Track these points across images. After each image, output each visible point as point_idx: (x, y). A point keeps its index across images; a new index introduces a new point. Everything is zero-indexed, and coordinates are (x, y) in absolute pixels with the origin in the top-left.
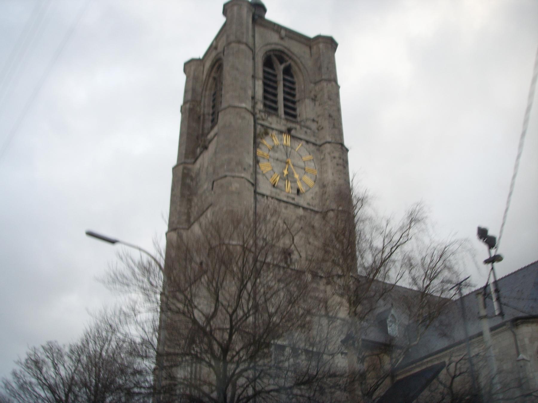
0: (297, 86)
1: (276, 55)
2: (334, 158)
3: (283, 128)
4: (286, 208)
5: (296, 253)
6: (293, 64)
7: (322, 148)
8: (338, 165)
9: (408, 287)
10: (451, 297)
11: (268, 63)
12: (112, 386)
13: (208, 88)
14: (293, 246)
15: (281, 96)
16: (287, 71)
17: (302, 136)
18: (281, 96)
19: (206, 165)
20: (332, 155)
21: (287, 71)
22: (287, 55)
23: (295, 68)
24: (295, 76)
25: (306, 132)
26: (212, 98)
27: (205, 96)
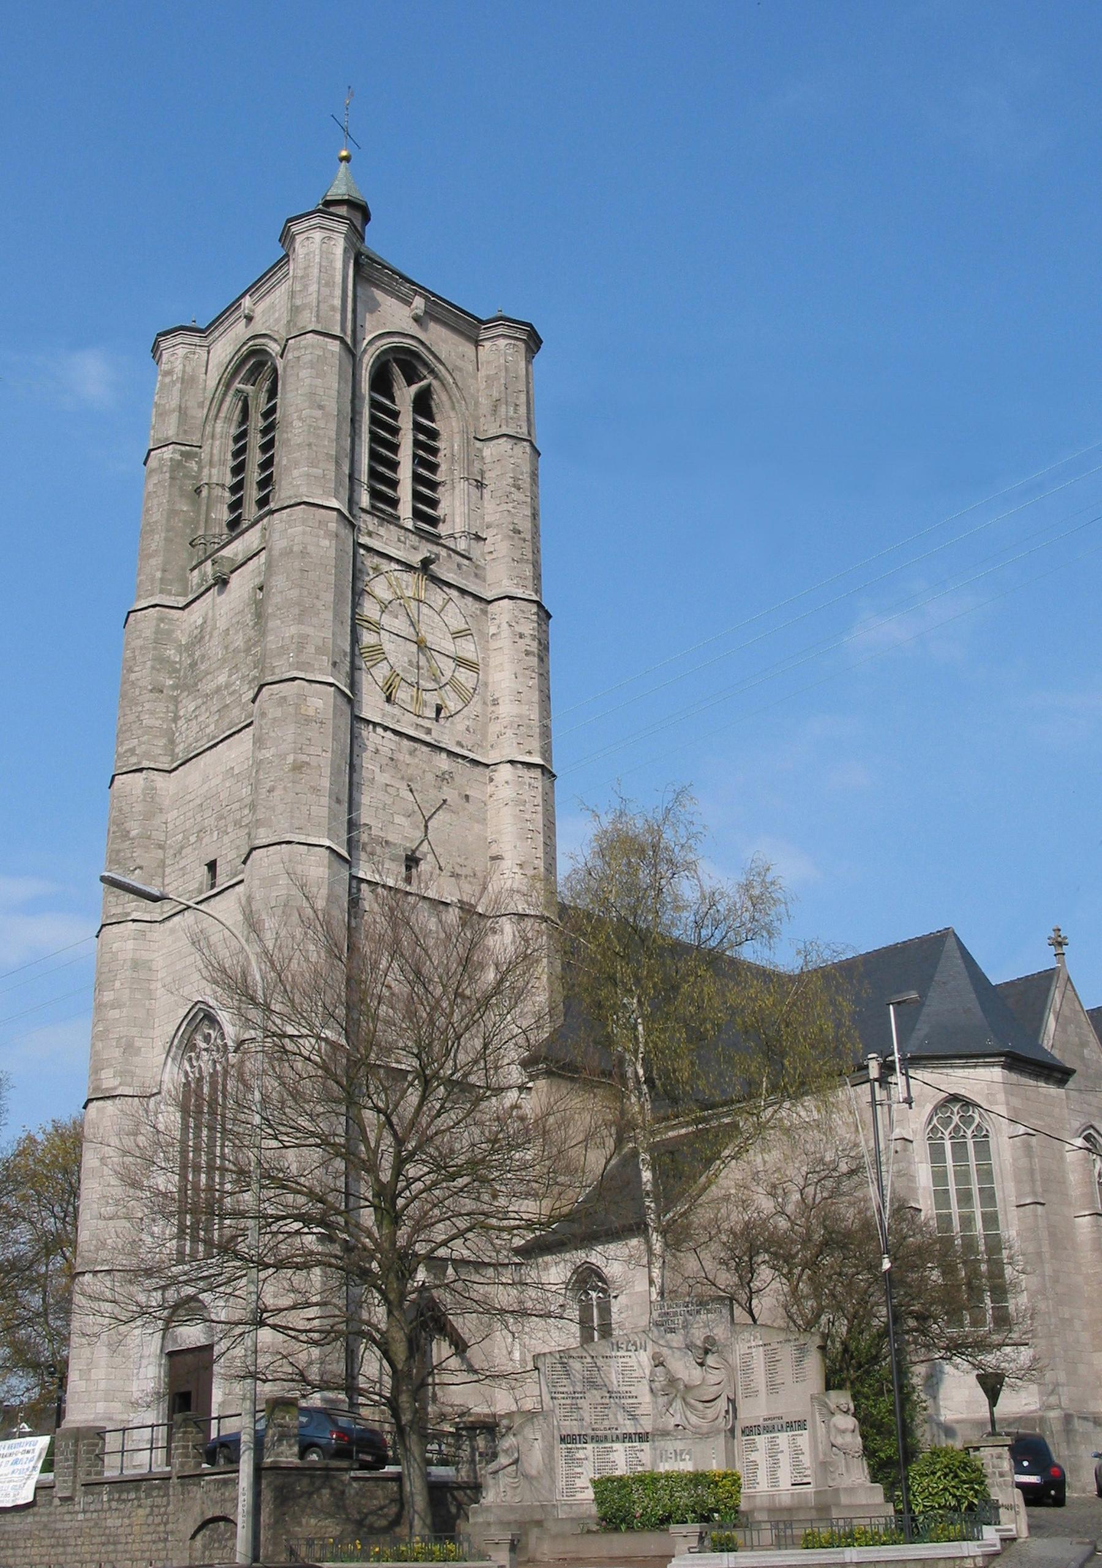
0: (440, 444)
1: (397, 361)
2: (521, 636)
3: (416, 559)
4: (412, 753)
5: (430, 857)
6: (435, 383)
7: (492, 608)
8: (527, 653)
9: (235, 463)
10: (131, 1426)
11: (381, 382)
12: (913, 992)
13: (222, 415)
14: (425, 847)
15: (405, 473)
16: (423, 404)
17: (449, 577)
18: (405, 473)
19: (222, 624)
20: (519, 629)
21: (423, 404)
22: (426, 365)
23: (440, 397)
24: (437, 417)
25: (459, 566)
26: (232, 447)
27: (213, 437)
